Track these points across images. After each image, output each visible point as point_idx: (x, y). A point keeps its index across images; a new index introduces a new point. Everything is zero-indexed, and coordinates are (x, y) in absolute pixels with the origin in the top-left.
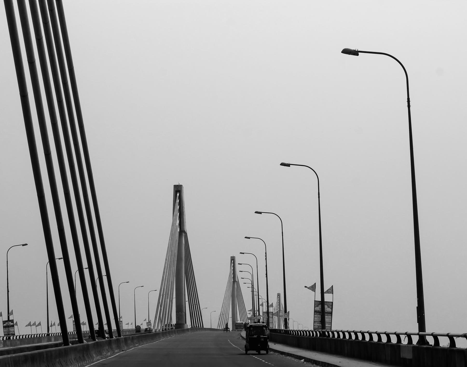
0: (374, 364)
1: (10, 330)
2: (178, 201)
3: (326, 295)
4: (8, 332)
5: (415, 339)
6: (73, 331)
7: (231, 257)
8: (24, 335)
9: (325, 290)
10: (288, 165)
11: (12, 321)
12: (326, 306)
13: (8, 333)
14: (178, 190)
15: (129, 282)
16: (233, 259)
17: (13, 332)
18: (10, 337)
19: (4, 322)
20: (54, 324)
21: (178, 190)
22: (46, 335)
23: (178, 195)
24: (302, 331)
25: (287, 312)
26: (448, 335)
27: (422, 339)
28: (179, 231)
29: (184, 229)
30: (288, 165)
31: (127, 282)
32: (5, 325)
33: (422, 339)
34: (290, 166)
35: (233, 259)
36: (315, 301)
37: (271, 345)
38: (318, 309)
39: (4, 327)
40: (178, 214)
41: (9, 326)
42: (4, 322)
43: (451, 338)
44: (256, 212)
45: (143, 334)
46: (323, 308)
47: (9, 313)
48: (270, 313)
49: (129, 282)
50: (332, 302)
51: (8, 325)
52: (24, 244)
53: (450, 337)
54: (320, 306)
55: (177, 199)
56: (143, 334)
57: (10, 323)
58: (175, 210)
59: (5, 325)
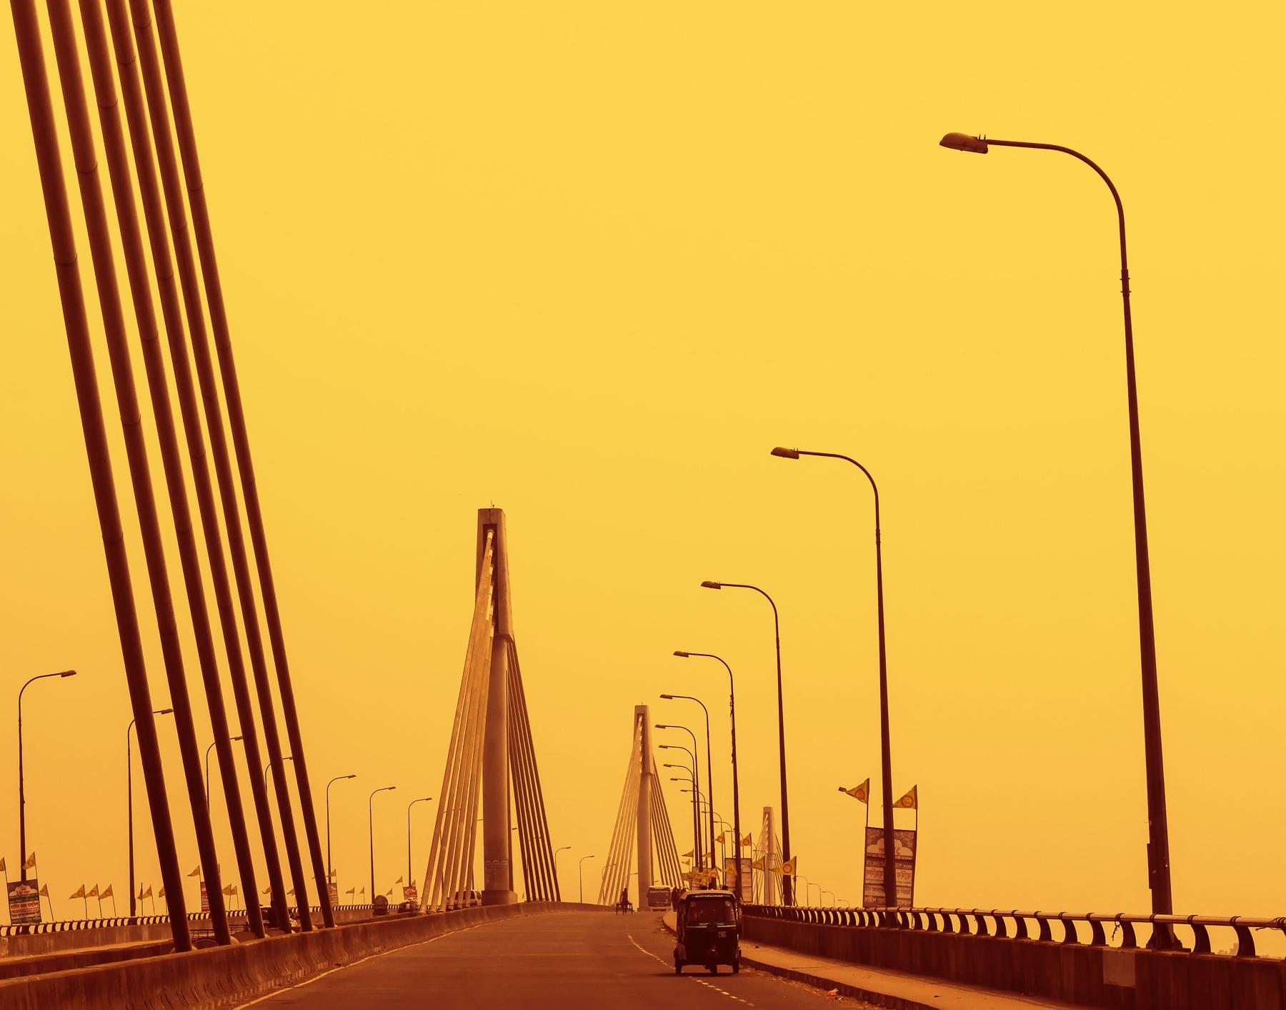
1: (28, 907)
3: (897, 812)
4: (23, 914)
5: (1144, 934)
8: (65, 922)
11: (34, 884)
12: (897, 843)
14: (490, 522)
20: (150, 892)
21: (490, 522)
22: (126, 922)
23: (490, 535)
24: (830, 910)
27: (1163, 933)
32: (13, 894)
33: (1163, 933)
34: (985, 151)
36: (867, 828)
38: (877, 849)
39: (10, 900)
41: (25, 898)
42: (11, 887)
43: (1243, 930)
47: (25, 862)
50: (915, 832)
51: (23, 893)
57: (28, 888)
59: (13, 894)
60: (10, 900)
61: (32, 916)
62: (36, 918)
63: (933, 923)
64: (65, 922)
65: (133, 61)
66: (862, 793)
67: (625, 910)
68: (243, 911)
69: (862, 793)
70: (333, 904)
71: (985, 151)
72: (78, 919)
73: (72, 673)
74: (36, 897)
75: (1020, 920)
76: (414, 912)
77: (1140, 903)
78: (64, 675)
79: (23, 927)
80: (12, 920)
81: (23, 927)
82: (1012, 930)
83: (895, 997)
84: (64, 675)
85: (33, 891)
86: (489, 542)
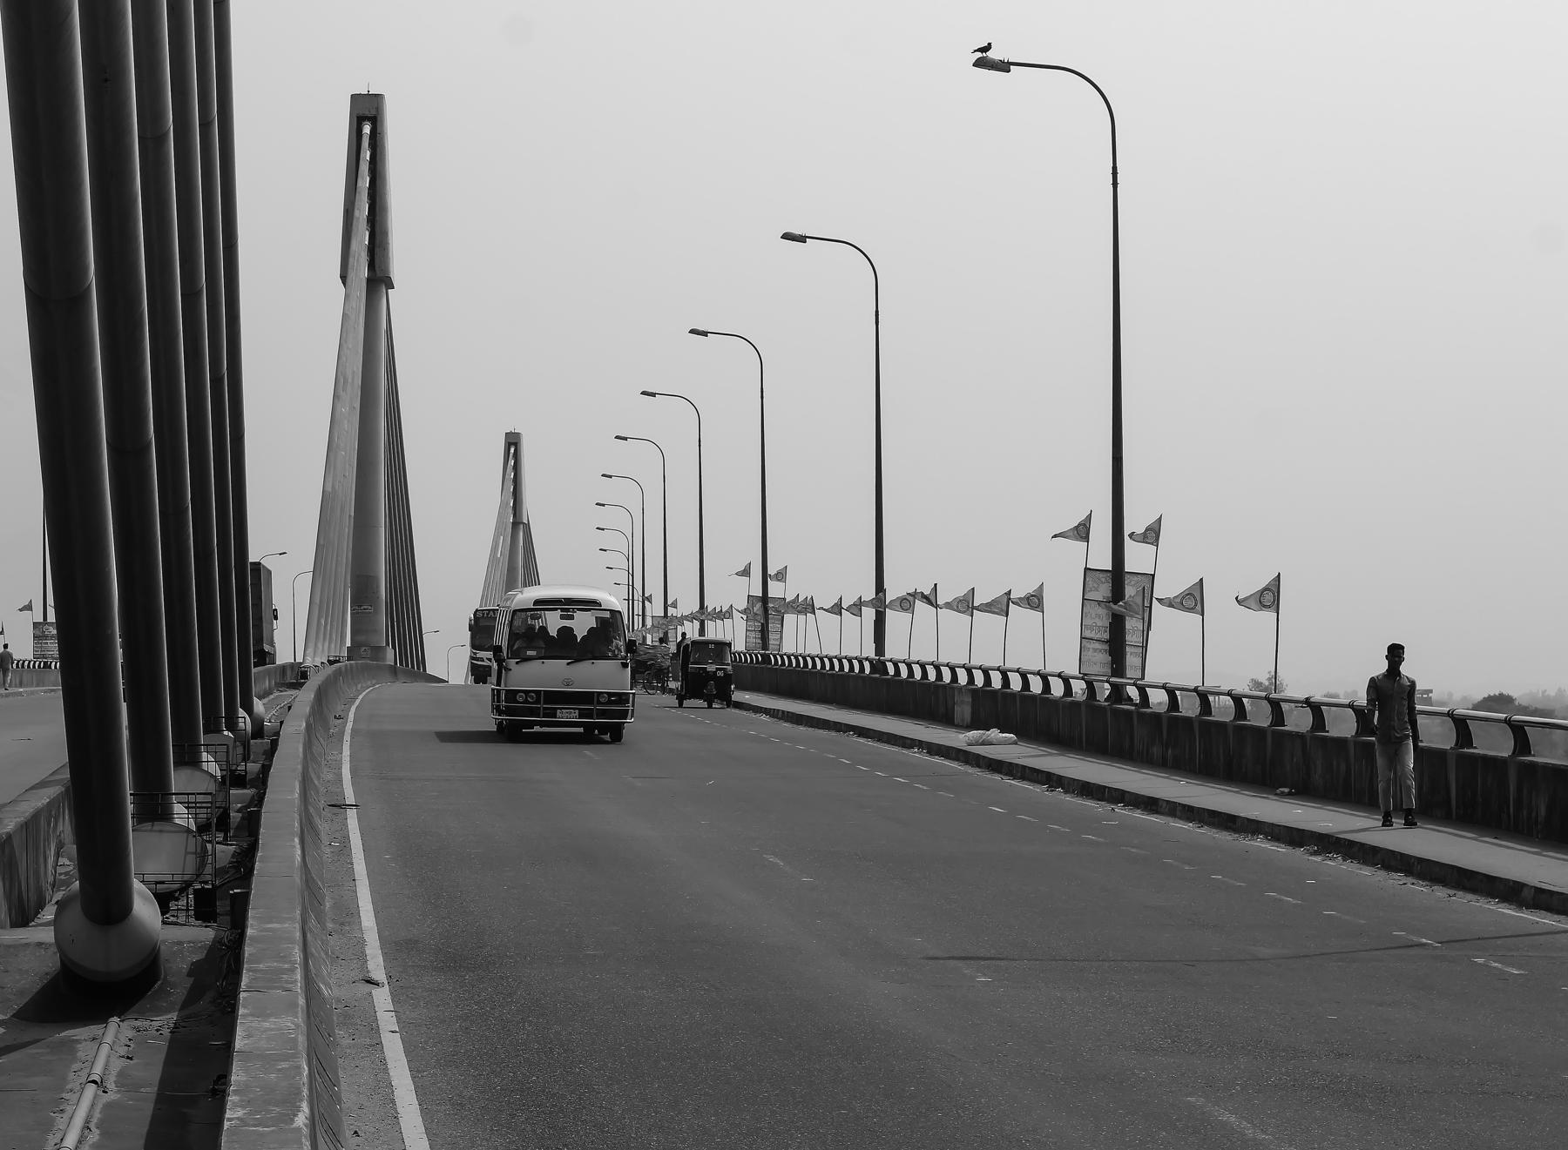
0: (1151, 772)
3: (1130, 546)
5: (1104, 691)
9: (771, 571)
10: (802, 239)
14: (513, 442)
16: (373, 113)
21: (513, 442)
23: (512, 450)
24: (809, 656)
26: (1164, 687)
27: (1118, 693)
28: (367, 243)
29: (386, 268)
30: (802, 239)
33: (1118, 693)
34: (805, 242)
35: (367, 113)
36: (1087, 569)
37: (738, 696)
38: (1103, 591)
40: (367, 233)
43: (1171, 692)
44: (787, 236)
46: (1117, 593)
48: (1127, 579)
50: (1153, 576)
53: (1314, 706)
54: (759, 605)
58: (354, 246)
63: (939, 675)
65: (376, 527)
70: (1067, 706)
71: (805, 242)
72: (23, 658)
75: (1045, 678)
77: (870, 651)
79: (44, 662)
81: (44, 662)
82: (947, 676)
83: (1272, 824)
86: (511, 455)
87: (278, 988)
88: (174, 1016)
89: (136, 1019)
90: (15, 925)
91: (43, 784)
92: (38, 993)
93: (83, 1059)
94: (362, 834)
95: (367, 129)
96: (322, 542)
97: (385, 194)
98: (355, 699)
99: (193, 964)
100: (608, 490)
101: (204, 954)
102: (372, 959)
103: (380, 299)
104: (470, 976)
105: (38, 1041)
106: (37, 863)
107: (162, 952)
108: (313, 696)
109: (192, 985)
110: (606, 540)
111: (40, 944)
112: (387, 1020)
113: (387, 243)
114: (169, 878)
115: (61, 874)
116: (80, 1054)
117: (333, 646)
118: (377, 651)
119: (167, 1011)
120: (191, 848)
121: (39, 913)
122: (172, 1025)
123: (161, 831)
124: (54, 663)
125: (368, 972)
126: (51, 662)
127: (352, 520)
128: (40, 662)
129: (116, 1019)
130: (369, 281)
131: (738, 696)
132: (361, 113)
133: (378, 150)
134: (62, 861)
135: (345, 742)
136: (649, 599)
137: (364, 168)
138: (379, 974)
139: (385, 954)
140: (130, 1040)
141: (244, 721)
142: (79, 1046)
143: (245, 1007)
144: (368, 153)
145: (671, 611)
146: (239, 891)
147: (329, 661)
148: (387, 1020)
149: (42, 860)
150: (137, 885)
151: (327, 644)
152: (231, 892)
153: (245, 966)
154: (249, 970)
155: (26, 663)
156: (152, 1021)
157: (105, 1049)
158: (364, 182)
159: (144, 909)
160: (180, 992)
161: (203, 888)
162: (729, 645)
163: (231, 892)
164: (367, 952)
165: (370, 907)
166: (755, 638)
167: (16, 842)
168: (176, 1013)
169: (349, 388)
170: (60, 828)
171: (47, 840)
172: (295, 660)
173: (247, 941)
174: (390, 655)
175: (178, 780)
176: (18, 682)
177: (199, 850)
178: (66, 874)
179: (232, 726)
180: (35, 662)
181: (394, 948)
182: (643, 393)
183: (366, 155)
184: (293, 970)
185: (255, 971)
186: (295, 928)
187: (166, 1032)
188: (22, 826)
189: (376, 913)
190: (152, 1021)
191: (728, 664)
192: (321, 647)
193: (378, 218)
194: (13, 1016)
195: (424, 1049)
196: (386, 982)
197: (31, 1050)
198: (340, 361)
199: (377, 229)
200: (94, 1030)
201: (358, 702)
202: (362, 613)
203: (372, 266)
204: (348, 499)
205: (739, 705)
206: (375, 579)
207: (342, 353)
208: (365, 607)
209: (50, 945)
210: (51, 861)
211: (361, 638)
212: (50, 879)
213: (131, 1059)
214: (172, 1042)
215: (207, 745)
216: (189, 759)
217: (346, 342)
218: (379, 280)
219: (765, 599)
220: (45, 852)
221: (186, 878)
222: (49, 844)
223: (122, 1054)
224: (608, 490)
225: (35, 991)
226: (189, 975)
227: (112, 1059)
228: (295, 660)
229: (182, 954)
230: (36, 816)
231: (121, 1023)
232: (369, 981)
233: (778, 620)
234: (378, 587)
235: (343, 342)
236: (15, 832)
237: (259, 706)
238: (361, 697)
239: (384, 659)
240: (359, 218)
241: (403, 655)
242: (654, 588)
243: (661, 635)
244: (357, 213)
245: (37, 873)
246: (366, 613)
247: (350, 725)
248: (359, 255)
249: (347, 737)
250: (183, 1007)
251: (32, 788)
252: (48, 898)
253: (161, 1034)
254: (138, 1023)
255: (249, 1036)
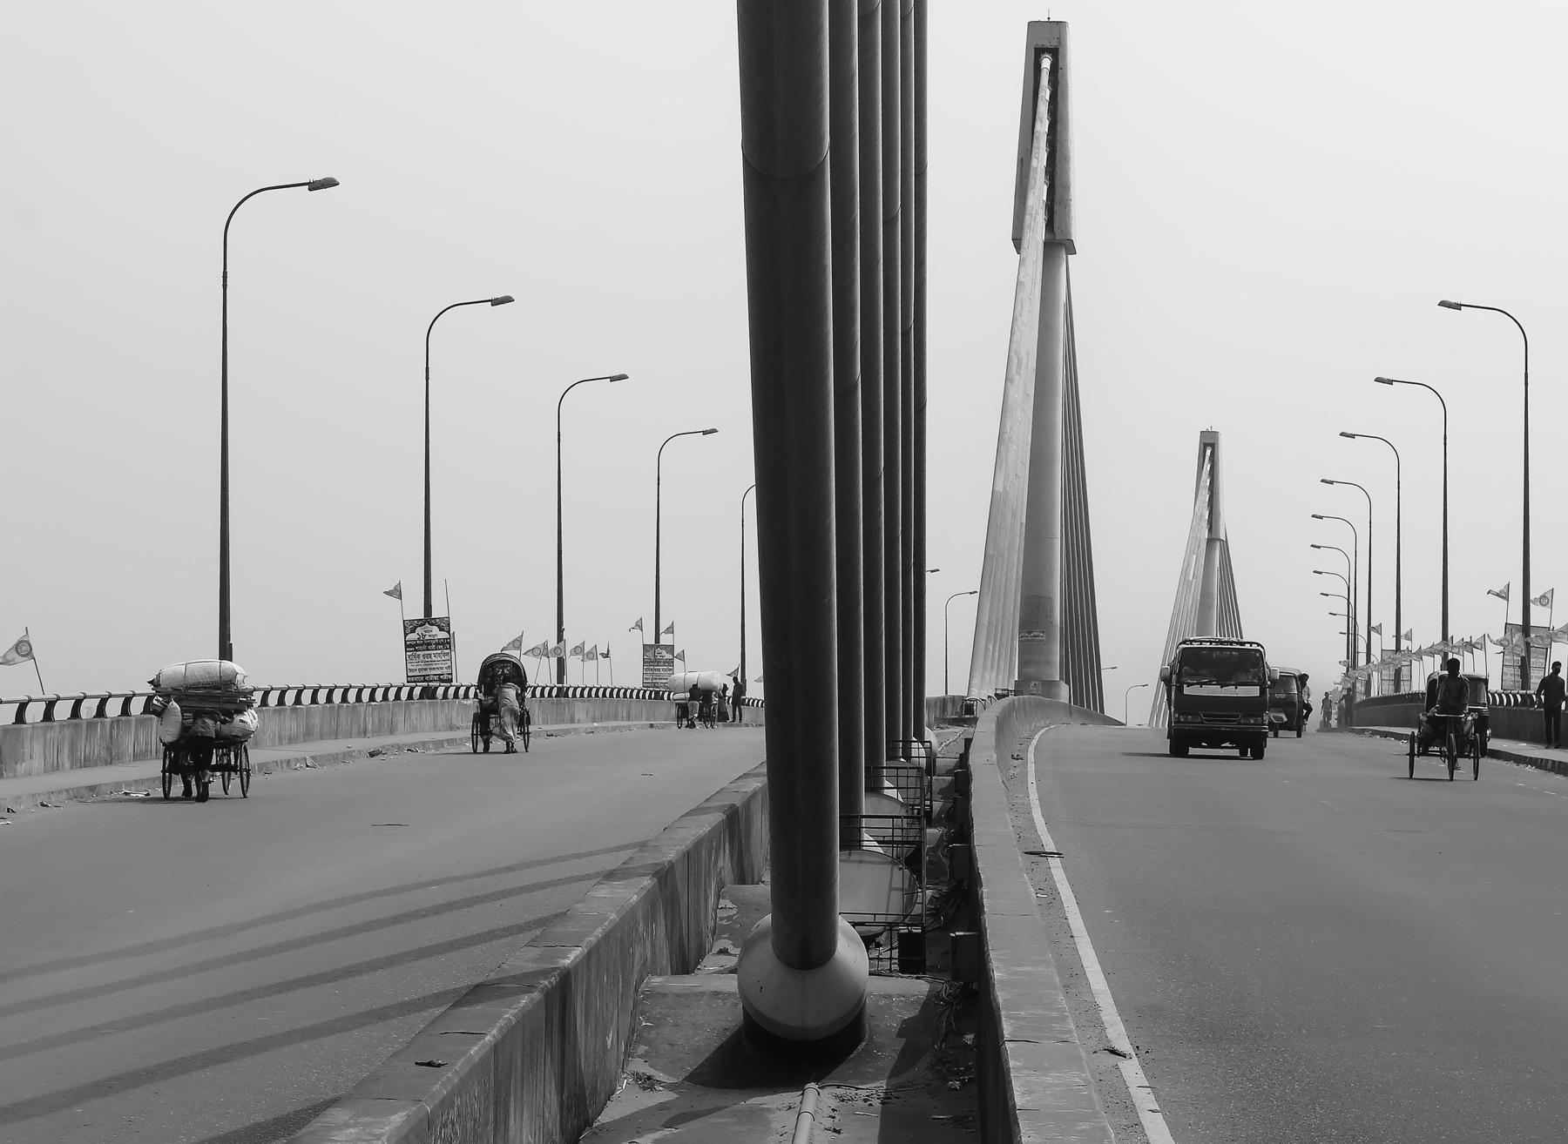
1: (434, 659)
2: (1207, 467)
4: (426, 669)
6: (640, 686)
7: (1032, 25)
8: (336, 687)
13: (424, 673)
14: (1209, 443)
15: (714, 431)
16: (1054, 43)
17: (445, 671)
18: (436, 688)
19: (410, 626)
20: (517, 644)
21: (1209, 443)
22: (137, 707)
23: (1208, 452)
25: (1449, 636)
31: (705, 433)
32: (412, 637)
35: (1047, 45)
40: (1046, 187)
42: (410, 626)
45: (1173, 694)
49: (714, 431)
51: (427, 637)
52: (318, 177)
55: (1205, 463)
56: (1173, 694)
57: (435, 630)
59: (412, 637)
60: (407, 646)
61: (665, 681)
62: (445, 677)
64: (336, 687)
66: (1504, 595)
67: (637, 625)
68: (468, 689)
69: (1504, 595)
73: (508, 300)
74: (671, 662)
76: (1021, 702)
78: (314, 186)
80: (408, 677)
84: (314, 186)
85: (668, 656)
87: (1049, 1038)
88: (882, 1084)
89: (838, 1087)
90: (674, 973)
91: (699, 811)
92: (714, 1052)
93: (781, 1130)
94: (1072, 886)
95: (1046, 63)
96: (991, 552)
97: (1067, 140)
98: (1030, 738)
99: (904, 1021)
100: (1329, 501)
101: (917, 1011)
102: (1111, 1026)
103: (1059, 267)
104: (1235, 1050)
105: (720, 1109)
106: (698, 902)
107: (867, 1005)
108: (994, 727)
109: (903, 1047)
110: (1324, 560)
111: (716, 994)
112: (1144, 1099)
113: (1069, 200)
114: (870, 918)
115: (722, 919)
116: (774, 1125)
117: (1000, 677)
118: (1050, 686)
119: (874, 1079)
120: (897, 883)
121: (699, 963)
122: (882, 1095)
123: (860, 862)
124: (666, 694)
125: (1109, 1041)
126: (664, 692)
127: (1024, 527)
128: (651, 692)
129: (813, 1085)
130: (1046, 244)
131: (1493, 744)
132: (1039, 45)
133: (1059, 88)
134: (723, 903)
135: (1029, 783)
136: (1379, 630)
137: (1043, 108)
138: (1124, 1045)
139: (1125, 1022)
140: (833, 1110)
141: (917, 750)
142: (772, 1115)
143: (1016, 1060)
144: (1048, 92)
145: (1404, 644)
146: (962, 933)
147: (996, 695)
148: (1144, 1099)
149: (702, 900)
150: (842, 923)
151: (994, 674)
152: (952, 935)
153: (1003, 1013)
154: (1009, 1017)
155: (635, 692)
156: (857, 1089)
157: (806, 1120)
158: (1043, 126)
159: (850, 952)
160: (889, 1055)
161: (910, 932)
162: (1486, 681)
163: (952, 935)
164: (1104, 1019)
165: (1098, 967)
166: (1513, 675)
167: (680, 873)
168: (885, 1082)
169: (1023, 371)
170: (721, 864)
171: (708, 875)
172: (946, 693)
173: (997, 986)
174: (1064, 693)
175: (867, 804)
176: (625, 715)
177: (906, 887)
178: (729, 918)
179: (908, 757)
180: (645, 691)
181: (1133, 1015)
182: (1378, 380)
183: (1045, 93)
184: (1064, 1019)
185: (1017, 1018)
186: (1052, 972)
187: (876, 1103)
188: (684, 854)
189: (1107, 974)
190: (857, 1089)
191: (1484, 705)
192: (988, 678)
193: (1058, 170)
194: (687, 1079)
195: (1194, 1131)
196: (1133, 1054)
197: (712, 1119)
198: (1015, 337)
199: (1058, 183)
200: (791, 1097)
201: (1034, 742)
202: (1032, 641)
203: (1210, 530)
204: (1020, 504)
205: (1496, 754)
206: (1050, 600)
207: (1016, 328)
208: (1036, 634)
209: (734, 994)
210: (712, 900)
211: (1031, 670)
212: (711, 923)
213: (838, 1132)
214: (886, 1117)
215: (890, 768)
216: (875, 788)
217: (1021, 315)
218: (1058, 243)
219: (1526, 628)
220: (706, 892)
221: (891, 919)
222: (710, 882)
223: (828, 1126)
224: (1329, 501)
225: (712, 1050)
226: (900, 1034)
227: (816, 1132)
228: (946, 693)
229: (891, 1009)
230: (698, 845)
231: (820, 1091)
232: (1114, 1052)
233: (1542, 654)
234: (1052, 609)
235: (1017, 314)
236: (677, 861)
237: (929, 735)
238: (1037, 737)
239: (1056, 696)
240: (1037, 168)
241: (1077, 697)
242: (1384, 615)
243: (1349, 685)
244: (1034, 163)
245: (697, 913)
246: (1037, 641)
247: (1031, 767)
248: (1037, 213)
249: (1031, 779)
250: (895, 1072)
251: (687, 814)
252: (708, 946)
253: (870, 1105)
254: (840, 1091)
255: (1029, 1092)
